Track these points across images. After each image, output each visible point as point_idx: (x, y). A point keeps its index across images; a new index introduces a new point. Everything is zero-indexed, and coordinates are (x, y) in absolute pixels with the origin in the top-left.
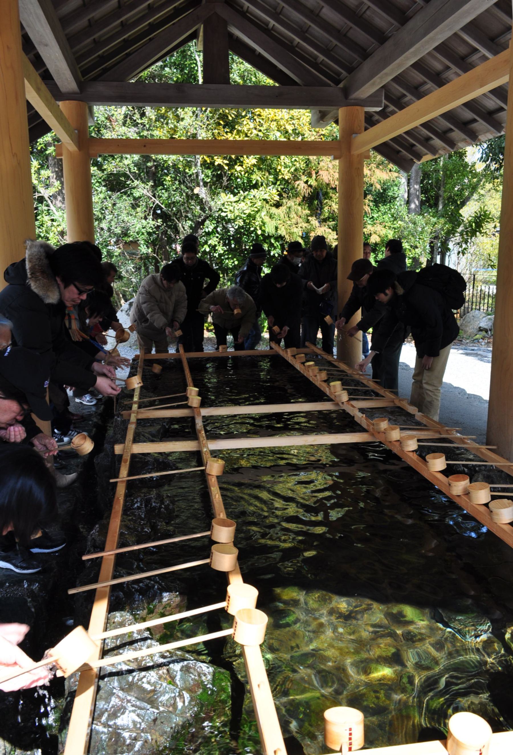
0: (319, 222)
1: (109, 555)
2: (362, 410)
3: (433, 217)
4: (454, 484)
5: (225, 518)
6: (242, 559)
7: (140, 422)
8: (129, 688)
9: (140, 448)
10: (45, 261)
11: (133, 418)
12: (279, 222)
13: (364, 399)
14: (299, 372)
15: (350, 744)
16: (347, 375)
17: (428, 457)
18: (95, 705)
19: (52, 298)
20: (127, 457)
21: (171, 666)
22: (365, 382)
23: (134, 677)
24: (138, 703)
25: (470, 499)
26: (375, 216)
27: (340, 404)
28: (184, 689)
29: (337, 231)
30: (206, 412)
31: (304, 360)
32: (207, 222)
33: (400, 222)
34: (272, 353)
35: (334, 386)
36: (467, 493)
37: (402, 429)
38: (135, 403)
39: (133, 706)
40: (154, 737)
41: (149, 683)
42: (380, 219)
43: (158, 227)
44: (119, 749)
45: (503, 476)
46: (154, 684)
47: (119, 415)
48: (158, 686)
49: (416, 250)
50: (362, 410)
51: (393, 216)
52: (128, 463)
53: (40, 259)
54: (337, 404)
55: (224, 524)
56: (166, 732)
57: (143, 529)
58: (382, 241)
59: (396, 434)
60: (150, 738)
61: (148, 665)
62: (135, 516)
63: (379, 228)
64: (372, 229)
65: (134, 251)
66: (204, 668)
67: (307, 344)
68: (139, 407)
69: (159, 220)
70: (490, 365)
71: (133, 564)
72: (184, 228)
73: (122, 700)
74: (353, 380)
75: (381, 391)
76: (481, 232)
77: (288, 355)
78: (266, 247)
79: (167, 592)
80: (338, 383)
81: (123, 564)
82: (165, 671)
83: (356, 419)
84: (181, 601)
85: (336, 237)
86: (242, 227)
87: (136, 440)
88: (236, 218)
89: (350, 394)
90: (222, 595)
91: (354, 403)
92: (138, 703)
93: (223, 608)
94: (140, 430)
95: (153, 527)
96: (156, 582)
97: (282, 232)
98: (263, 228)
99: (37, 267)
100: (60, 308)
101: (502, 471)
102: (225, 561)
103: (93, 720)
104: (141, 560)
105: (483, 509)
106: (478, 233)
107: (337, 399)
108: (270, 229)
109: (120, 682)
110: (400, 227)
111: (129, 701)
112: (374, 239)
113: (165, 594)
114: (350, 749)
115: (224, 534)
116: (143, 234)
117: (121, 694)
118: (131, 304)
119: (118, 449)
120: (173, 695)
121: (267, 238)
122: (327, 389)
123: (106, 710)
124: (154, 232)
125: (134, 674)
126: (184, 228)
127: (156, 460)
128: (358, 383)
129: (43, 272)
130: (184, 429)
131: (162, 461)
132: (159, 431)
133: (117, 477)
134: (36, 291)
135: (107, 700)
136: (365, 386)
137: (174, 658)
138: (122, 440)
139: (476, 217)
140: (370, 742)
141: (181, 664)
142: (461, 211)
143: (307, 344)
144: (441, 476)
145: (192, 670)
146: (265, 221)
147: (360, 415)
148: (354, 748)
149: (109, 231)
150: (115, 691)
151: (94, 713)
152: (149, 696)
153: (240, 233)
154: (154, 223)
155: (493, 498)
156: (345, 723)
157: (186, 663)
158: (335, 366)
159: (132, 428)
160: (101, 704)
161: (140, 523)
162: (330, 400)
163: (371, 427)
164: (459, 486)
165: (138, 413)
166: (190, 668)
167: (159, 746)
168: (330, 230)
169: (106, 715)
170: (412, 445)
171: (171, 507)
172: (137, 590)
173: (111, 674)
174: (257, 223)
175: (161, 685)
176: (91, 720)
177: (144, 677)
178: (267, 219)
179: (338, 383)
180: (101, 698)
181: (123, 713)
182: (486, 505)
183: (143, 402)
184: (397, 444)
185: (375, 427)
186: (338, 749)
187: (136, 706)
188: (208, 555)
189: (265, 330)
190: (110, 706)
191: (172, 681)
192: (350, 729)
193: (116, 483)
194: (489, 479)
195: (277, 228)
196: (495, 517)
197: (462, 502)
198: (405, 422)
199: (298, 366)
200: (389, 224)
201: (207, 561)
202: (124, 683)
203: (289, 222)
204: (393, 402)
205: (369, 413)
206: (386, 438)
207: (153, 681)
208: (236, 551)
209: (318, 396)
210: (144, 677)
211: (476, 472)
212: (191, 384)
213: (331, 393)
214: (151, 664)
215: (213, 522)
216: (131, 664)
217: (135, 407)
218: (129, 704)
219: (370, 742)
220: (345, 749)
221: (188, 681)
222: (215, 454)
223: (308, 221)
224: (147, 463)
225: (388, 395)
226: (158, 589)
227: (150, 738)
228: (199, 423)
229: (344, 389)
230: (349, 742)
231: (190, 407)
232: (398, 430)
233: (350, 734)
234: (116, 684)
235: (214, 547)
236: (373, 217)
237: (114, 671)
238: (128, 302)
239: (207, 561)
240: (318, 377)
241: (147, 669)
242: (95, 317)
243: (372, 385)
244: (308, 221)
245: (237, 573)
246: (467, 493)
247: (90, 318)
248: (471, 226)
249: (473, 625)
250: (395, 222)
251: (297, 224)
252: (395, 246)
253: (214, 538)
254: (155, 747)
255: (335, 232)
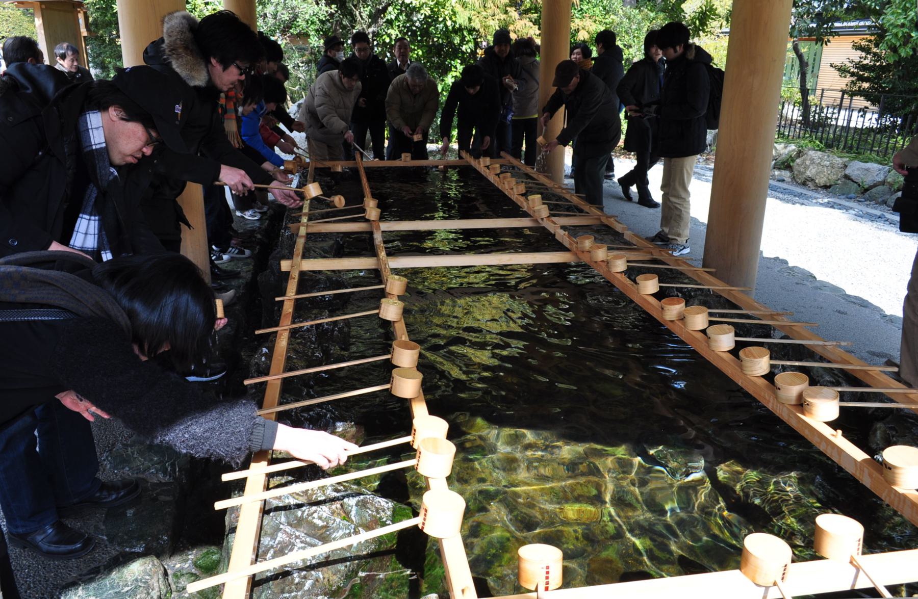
0: (520, 14)
1: (274, 379)
2: (564, 228)
3: (651, 10)
4: (667, 307)
5: (407, 339)
6: (427, 388)
7: (309, 236)
8: (298, 523)
9: (310, 265)
10: (189, 35)
11: (303, 231)
12: (473, 13)
13: (567, 216)
14: (493, 185)
15: (547, 583)
16: (547, 189)
17: (638, 279)
18: (259, 542)
19: (199, 80)
20: (295, 275)
21: (346, 500)
22: (567, 197)
23: (304, 512)
24: (308, 539)
25: (685, 324)
26: (585, 8)
27: (540, 221)
28: (360, 526)
29: (539, 25)
30: (385, 226)
31: (498, 172)
32: (390, 9)
33: (612, 16)
34: (462, 163)
35: (533, 200)
36: (682, 319)
37: (609, 249)
38: (305, 214)
39: (302, 542)
40: (326, 576)
41: (320, 518)
42: (590, 12)
43: (332, 15)
44: (287, 588)
45: (722, 300)
46: (326, 520)
47: (286, 228)
48: (331, 522)
49: (630, 50)
50: (564, 228)
51: (605, 9)
52: (296, 280)
53: (182, 32)
54: (536, 221)
55: (406, 346)
56: (339, 571)
57: (313, 353)
58: (591, 38)
59: (601, 254)
60: (321, 576)
61: (319, 499)
62: (304, 339)
63: (588, 23)
64: (581, 24)
65: (303, 46)
66: (383, 503)
67: (502, 153)
68: (310, 219)
69: (333, 6)
70: (709, 186)
71: (302, 391)
72: (361, 17)
73: (289, 536)
74: (554, 195)
75: (586, 207)
76: (704, 31)
77: (482, 165)
78: (457, 40)
79: (340, 421)
80: (538, 197)
81: (290, 389)
82: (339, 506)
83: (557, 237)
84: (357, 432)
85: (538, 32)
86: (430, 17)
87: (306, 255)
88: (422, 6)
89: (550, 209)
90: (407, 427)
91: (554, 219)
92: (308, 539)
93: (409, 443)
94: (311, 244)
95: (326, 352)
96: (329, 411)
97: (476, 24)
98: (454, 19)
99: (178, 42)
100: (210, 91)
101: (721, 296)
102: (407, 386)
103: (257, 556)
104: (312, 387)
105: (700, 336)
106: (701, 33)
107: (536, 214)
108: (462, 19)
109: (287, 517)
110: (612, 23)
111: (297, 537)
112: (582, 36)
113: (338, 424)
114: (547, 589)
115: (406, 358)
116: (313, 23)
117: (288, 529)
118: (299, 106)
119: (285, 265)
120: (348, 531)
121: (458, 30)
122: (525, 204)
123: (272, 547)
124: (328, 20)
125: (304, 508)
126: (361, 17)
127: (329, 278)
128: (560, 198)
129: (186, 48)
130: (361, 245)
131: (334, 279)
132: (331, 247)
133: (283, 294)
134: (178, 70)
135: (273, 537)
136: (567, 200)
137: (349, 492)
138: (290, 256)
139: (702, 12)
140: (568, 581)
141: (357, 499)
142: (683, 6)
143: (502, 153)
144: (653, 300)
145: (369, 506)
146: (456, 9)
147: (562, 232)
148: (551, 587)
149: (275, 18)
150: (281, 526)
151: (258, 550)
152: (321, 532)
153: (427, 23)
154: (327, 9)
155: (711, 323)
156: (540, 561)
157: (362, 497)
158: (534, 179)
159: (300, 243)
160: (266, 541)
161: (310, 346)
162: (525, 215)
163: (575, 245)
164: (673, 311)
165: (307, 226)
166: (367, 502)
167: (331, 586)
168: (531, 24)
169: (272, 551)
170: (620, 266)
171: (346, 329)
172: (306, 419)
173: (278, 509)
174: (446, 12)
175: (335, 520)
176: (254, 557)
177: (315, 512)
178: (458, 8)
179: (538, 197)
180: (266, 534)
181: (291, 550)
182: (704, 331)
183: (314, 215)
184: (603, 265)
185: (579, 246)
186: (533, 589)
187: (305, 543)
188: (388, 379)
189: (454, 139)
190: (277, 542)
191: (347, 516)
192: (548, 567)
193: (283, 302)
194: (706, 304)
195: (470, 19)
196: (713, 344)
197: (677, 330)
198: (612, 242)
199: (492, 178)
200: (599, 18)
201: (387, 386)
202: (292, 518)
203: (484, 13)
204: (600, 219)
205: (573, 231)
206: (591, 258)
207: (325, 515)
208: (421, 376)
209: (515, 211)
210: (315, 512)
211: (691, 297)
212: (369, 195)
213: (529, 207)
214: (323, 498)
215: (394, 344)
216: (301, 498)
217: (304, 220)
218: (298, 541)
219: (568, 581)
220: (541, 589)
221: (365, 516)
222: (397, 271)
223: (506, 12)
224: (318, 282)
225: (594, 211)
226: (331, 418)
227: (321, 576)
228: (378, 238)
229: (544, 204)
230: (545, 581)
231: (367, 221)
232: (606, 248)
233: (548, 573)
234: (283, 519)
235: (394, 371)
236: (582, 9)
237: (281, 505)
238: (296, 104)
239: (387, 386)
240: (515, 190)
241: (318, 503)
242: (250, 104)
243: (575, 200)
244: (506, 12)
245: (421, 401)
246: (682, 319)
247: (243, 105)
248: (695, 23)
249: (559, 503)
250: (607, 16)
251: (494, 15)
252: (606, 38)
253: (394, 362)
254: (327, 586)
255: (537, 27)
